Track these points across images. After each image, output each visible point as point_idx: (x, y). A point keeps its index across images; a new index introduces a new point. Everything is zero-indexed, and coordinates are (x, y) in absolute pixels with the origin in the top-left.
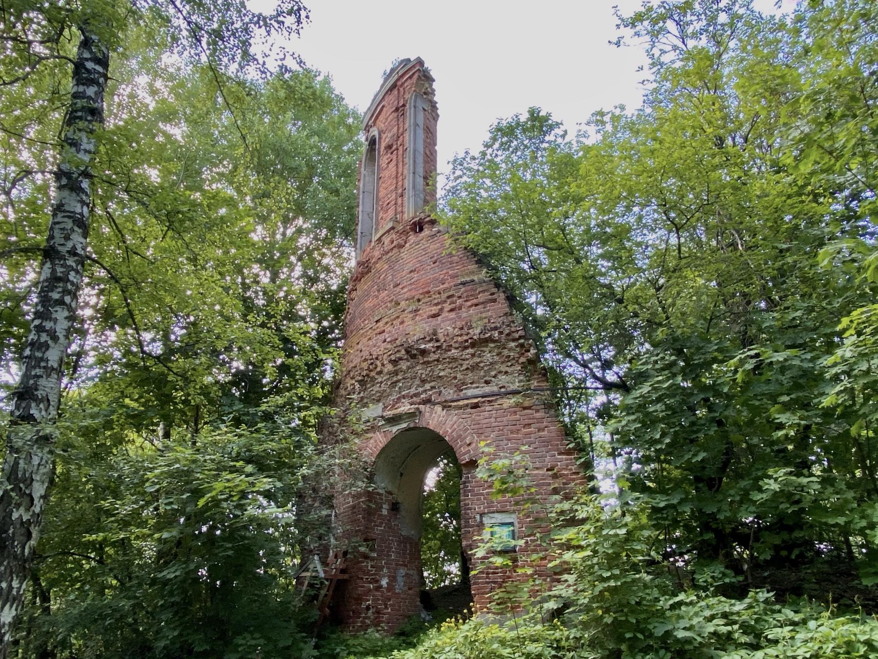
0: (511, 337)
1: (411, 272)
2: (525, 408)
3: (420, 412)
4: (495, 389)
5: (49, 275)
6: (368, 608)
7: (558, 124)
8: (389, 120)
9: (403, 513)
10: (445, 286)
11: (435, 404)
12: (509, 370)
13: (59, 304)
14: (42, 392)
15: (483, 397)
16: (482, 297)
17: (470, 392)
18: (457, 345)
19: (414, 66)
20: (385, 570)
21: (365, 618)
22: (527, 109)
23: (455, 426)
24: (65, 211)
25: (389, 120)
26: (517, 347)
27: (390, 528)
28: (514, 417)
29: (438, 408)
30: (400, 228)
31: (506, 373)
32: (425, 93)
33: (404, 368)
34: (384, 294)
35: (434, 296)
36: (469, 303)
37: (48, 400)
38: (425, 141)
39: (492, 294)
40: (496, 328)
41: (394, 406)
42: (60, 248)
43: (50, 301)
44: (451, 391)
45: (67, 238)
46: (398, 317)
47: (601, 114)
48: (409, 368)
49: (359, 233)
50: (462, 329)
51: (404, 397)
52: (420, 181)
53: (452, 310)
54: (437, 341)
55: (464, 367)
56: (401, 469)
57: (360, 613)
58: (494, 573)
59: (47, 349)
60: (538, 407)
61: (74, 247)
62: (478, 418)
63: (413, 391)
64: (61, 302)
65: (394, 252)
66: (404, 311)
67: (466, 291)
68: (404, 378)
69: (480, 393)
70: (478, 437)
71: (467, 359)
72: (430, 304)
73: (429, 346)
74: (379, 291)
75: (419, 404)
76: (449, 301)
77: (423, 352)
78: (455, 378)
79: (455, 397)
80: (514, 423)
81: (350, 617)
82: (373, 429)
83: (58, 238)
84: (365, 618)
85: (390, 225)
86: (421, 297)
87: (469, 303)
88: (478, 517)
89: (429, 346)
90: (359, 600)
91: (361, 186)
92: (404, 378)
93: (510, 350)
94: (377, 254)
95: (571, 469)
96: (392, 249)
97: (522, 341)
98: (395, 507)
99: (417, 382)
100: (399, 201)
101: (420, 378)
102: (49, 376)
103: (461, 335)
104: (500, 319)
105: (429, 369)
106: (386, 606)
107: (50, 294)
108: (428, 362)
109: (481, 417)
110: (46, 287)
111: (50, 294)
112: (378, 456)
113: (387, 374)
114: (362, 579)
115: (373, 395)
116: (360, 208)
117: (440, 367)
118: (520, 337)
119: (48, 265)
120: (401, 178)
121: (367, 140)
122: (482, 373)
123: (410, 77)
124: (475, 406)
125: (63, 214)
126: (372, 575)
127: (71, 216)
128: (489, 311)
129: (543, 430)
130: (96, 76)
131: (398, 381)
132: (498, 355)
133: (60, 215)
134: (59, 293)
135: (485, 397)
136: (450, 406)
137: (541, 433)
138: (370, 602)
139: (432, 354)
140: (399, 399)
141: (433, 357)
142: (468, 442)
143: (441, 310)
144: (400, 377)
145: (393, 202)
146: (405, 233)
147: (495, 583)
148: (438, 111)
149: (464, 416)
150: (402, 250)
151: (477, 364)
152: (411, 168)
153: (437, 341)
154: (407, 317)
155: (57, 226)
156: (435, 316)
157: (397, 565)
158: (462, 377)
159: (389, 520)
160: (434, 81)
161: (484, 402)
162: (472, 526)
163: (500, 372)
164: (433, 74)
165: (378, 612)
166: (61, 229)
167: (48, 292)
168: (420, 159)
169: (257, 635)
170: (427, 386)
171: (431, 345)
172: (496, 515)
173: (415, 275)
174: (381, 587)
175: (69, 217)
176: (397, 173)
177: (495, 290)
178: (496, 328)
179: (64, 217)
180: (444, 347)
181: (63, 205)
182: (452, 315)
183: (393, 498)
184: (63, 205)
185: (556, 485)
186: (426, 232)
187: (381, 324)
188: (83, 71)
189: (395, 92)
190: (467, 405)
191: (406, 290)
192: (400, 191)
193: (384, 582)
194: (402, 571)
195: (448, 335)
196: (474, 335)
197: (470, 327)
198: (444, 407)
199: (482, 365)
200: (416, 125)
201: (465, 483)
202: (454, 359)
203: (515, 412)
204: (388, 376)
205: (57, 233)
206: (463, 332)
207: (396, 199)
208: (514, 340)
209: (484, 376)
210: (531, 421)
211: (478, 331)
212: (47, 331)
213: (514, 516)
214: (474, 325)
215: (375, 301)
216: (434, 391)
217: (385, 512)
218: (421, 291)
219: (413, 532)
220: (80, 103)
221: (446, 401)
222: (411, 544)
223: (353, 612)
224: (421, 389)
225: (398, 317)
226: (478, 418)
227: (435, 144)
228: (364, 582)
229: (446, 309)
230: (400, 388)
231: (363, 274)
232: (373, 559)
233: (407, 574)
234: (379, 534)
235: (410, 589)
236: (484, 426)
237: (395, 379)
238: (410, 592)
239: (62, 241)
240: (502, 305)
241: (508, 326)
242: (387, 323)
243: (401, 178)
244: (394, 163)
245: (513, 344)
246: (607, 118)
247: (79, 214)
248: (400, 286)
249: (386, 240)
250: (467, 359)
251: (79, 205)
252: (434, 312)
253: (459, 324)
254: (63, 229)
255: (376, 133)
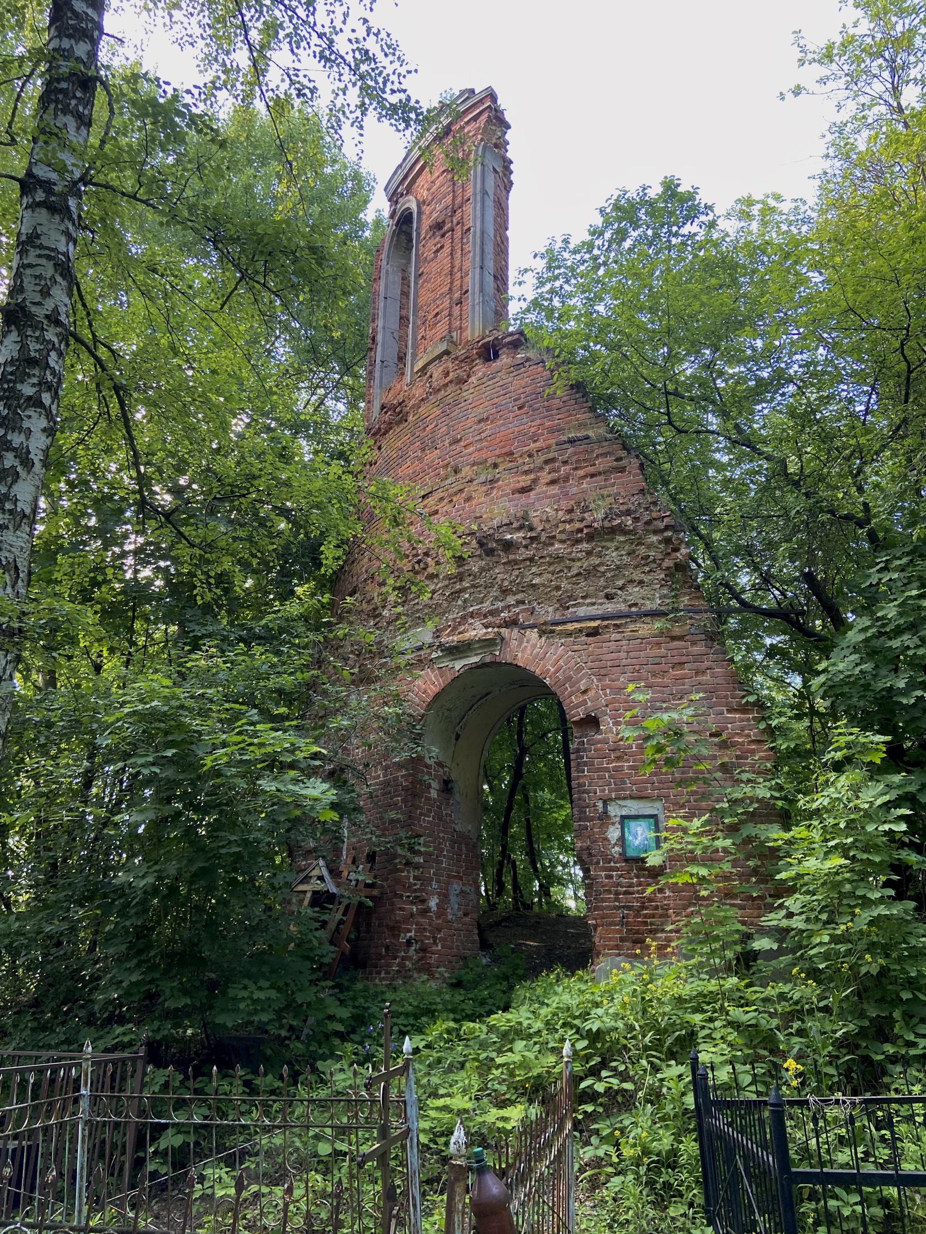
0: (651, 528)
1: (480, 421)
2: (673, 638)
3: (503, 639)
4: (623, 607)
5: (16, 355)
6: (409, 943)
7: (709, 208)
8: (438, 184)
9: (457, 797)
10: (538, 444)
11: (525, 628)
12: (646, 578)
13: (34, 405)
14: (7, 554)
15: (603, 618)
16: (602, 464)
17: (582, 611)
18: (564, 537)
19: (481, 101)
20: (434, 885)
21: (404, 959)
22: (662, 179)
23: (561, 662)
24: (41, 247)
25: (438, 184)
26: (660, 542)
27: (440, 819)
28: (656, 652)
29: (533, 634)
30: (461, 352)
31: (641, 582)
32: (496, 146)
33: (475, 569)
34: (432, 456)
35: (520, 461)
36: (581, 473)
37: (16, 568)
38: (495, 220)
39: (619, 459)
40: (628, 513)
41: (455, 629)
42: (33, 309)
43: (18, 399)
44: (550, 609)
45: (45, 293)
46: (461, 491)
47: (750, 202)
48: (482, 569)
49: (378, 361)
50: (571, 511)
51: (472, 615)
52: (489, 280)
53: (553, 482)
54: (531, 529)
55: (575, 571)
56: (458, 728)
57: (397, 951)
58: (626, 893)
59: (15, 481)
60: (696, 638)
61: (56, 310)
62: (599, 651)
63: (486, 606)
64: (36, 402)
65: (449, 390)
66: (471, 481)
67: (575, 453)
68: (473, 586)
69: (600, 612)
70: (599, 680)
71: (580, 559)
72: (515, 471)
73: (517, 536)
74: (423, 450)
75: (500, 627)
76: (547, 468)
77: (508, 546)
78: (558, 588)
79: (558, 617)
80: (657, 660)
81: (380, 957)
82: (421, 663)
83: (31, 293)
84: (404, 959)
85: (443, 347)
86: (499, 460)
87: (581, 473)
88: (600, 805)
89: (517, 536)
90: (395, 930)
91: (382, 288)
92: (473, 586)
93: (650, 546)
94: (418, 392)
95: (748, 736)
96: (446, 385)
97: (669, 533)
98: (447, 786)
99: (495, 592)
100: (456, 311)
101: (501, 587)
102: (17, 527)
103: (570, 521)
104: (633, 499)
105: (516, 573)
106: (435, 939)
107: (19, 387)
108: (516, 562)
109: (605, 650)
110: (12, 373)
111: (19, 387)
112: (429, 706)
113: (445, 578)
114: (401, 896)
115: (418, 611)
116: (380, 323)
117: (534, 569)
118: (667, 528)
119: (14, 336)
120: (458, 275)
121: (392, 216)
122: (602, 582)
123: (475, 119)
124: (594, 633)
125: (38, 252)
126: (416, 891)
127: (51, 255)
128: (613, 485)
129: (703, 673)
130: (90, 25)
131: (463, 590)
132: (629, 554)
133: (33, 252)
134: (34, 385)
135: (607, 619)
136: (552, 632)
137: (701, 678)
138: (412, 934)
139: (523, 550)
140: (464, 618)
141: (523, 554)
142: (583, 688)
143: (535, 481)
144: (466, 584)
145: (446, 312)
146: (467, 360)
147: (629, 908)
148: (513, 177)
149: (576, 648)
150: (465, 387)
151: (595, 567)
152: (478, 259)
153: (531, 529)
154: (478, 492)
155: (28, 271)
156: (524, 490)
157: (449, 876)
158: (569, 587)
159: (439, 807)
160: (509, 127)
161: (607, 627)
162: (591, 819)
163: (631, 581)
164: (508, 117)
165: (424, 950)
166: (36, 277)
167: (15, 382)
168: (490, 248)
169: (265, 984)
170: (511, 600)
171: (521, 534)
172: (629, 803)
173: (488, 428)
174: (428, 910)
175: (49, 258)
176: (453, 267)
177: (623, 453)
178: (628, 513)
179: (39, 256)
180: (543, 539)
181: (38, 236)
182: (555, 490)
183: (445, 773)
184: (38, 236)
185: (726, 759)
186: (505, 359)
187: (430, 501)
188: (69, 15)
189: (449, 140)
190: (581, 631)
191: (471, 449)
192: (457, 295)
193: (433, 903)
194: (455, 886)
195: (548, 521)
196: (594, 521)
197: (586, 509)
198: (542, 633)
199: (602, 569)
200: (484, 193)
201: (578, 751)
202: (559, 559)
203: (658, 644)
204: (447, 582)
205: (29, 284)
206: (573, 516)
207: (451, 308)
208: (656, 532)
209: (605, 587)
210: (684, 659)
211: (600, 515)
212: (14, 450)
213: (658, 805)
214: (592, 506)
215: (417, 466)
216: (522, 607)
217: (434, 794)
218: (497, 452)
219: (470, 827)
220: (65, 67)
221: (545, 623)
222: (467, 845)
223: (387, 948)
224: (500, 605)
225: (461, 491)
226: (599, 651)
227: (507, 229)
228: (405, 903)
229: (543, 481)
230: (465, 601)
231: (390, 426)
232: (417, 866)
233: (462, 892)
234: (426, 828)
235: (466, 915)
236: (609, 664)
237: (458, 587)
238: (467, 919)
239: (38, 298)
240: (632, 478)
241: (647, 509)
242: (442, 499)
243: (458, 275)
244: (447, 250)
245: (654, 538)
246: (756, 210)
247: (63, 254)
248: (462, 444)
249: (436, 371)
250: (580, 559)
251: (63, 239)
252: (522, 484)
253: (565, 504)
254: (39, 277)
255: (414, 206)
